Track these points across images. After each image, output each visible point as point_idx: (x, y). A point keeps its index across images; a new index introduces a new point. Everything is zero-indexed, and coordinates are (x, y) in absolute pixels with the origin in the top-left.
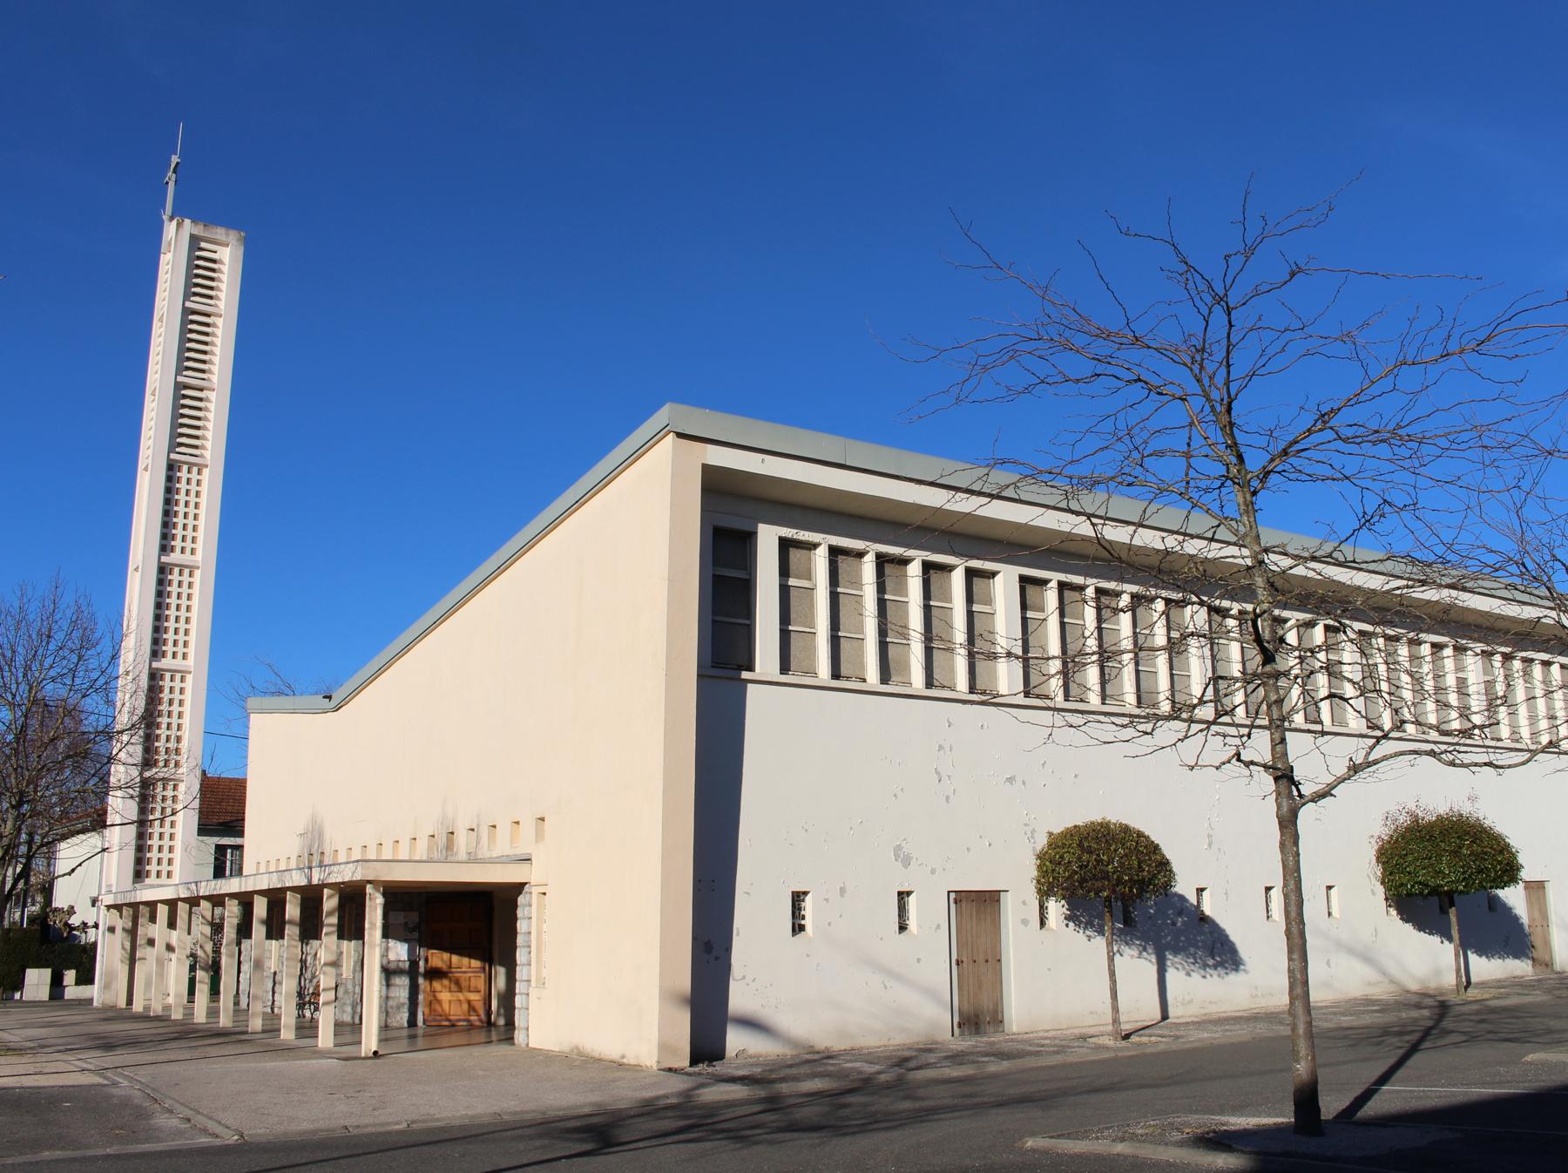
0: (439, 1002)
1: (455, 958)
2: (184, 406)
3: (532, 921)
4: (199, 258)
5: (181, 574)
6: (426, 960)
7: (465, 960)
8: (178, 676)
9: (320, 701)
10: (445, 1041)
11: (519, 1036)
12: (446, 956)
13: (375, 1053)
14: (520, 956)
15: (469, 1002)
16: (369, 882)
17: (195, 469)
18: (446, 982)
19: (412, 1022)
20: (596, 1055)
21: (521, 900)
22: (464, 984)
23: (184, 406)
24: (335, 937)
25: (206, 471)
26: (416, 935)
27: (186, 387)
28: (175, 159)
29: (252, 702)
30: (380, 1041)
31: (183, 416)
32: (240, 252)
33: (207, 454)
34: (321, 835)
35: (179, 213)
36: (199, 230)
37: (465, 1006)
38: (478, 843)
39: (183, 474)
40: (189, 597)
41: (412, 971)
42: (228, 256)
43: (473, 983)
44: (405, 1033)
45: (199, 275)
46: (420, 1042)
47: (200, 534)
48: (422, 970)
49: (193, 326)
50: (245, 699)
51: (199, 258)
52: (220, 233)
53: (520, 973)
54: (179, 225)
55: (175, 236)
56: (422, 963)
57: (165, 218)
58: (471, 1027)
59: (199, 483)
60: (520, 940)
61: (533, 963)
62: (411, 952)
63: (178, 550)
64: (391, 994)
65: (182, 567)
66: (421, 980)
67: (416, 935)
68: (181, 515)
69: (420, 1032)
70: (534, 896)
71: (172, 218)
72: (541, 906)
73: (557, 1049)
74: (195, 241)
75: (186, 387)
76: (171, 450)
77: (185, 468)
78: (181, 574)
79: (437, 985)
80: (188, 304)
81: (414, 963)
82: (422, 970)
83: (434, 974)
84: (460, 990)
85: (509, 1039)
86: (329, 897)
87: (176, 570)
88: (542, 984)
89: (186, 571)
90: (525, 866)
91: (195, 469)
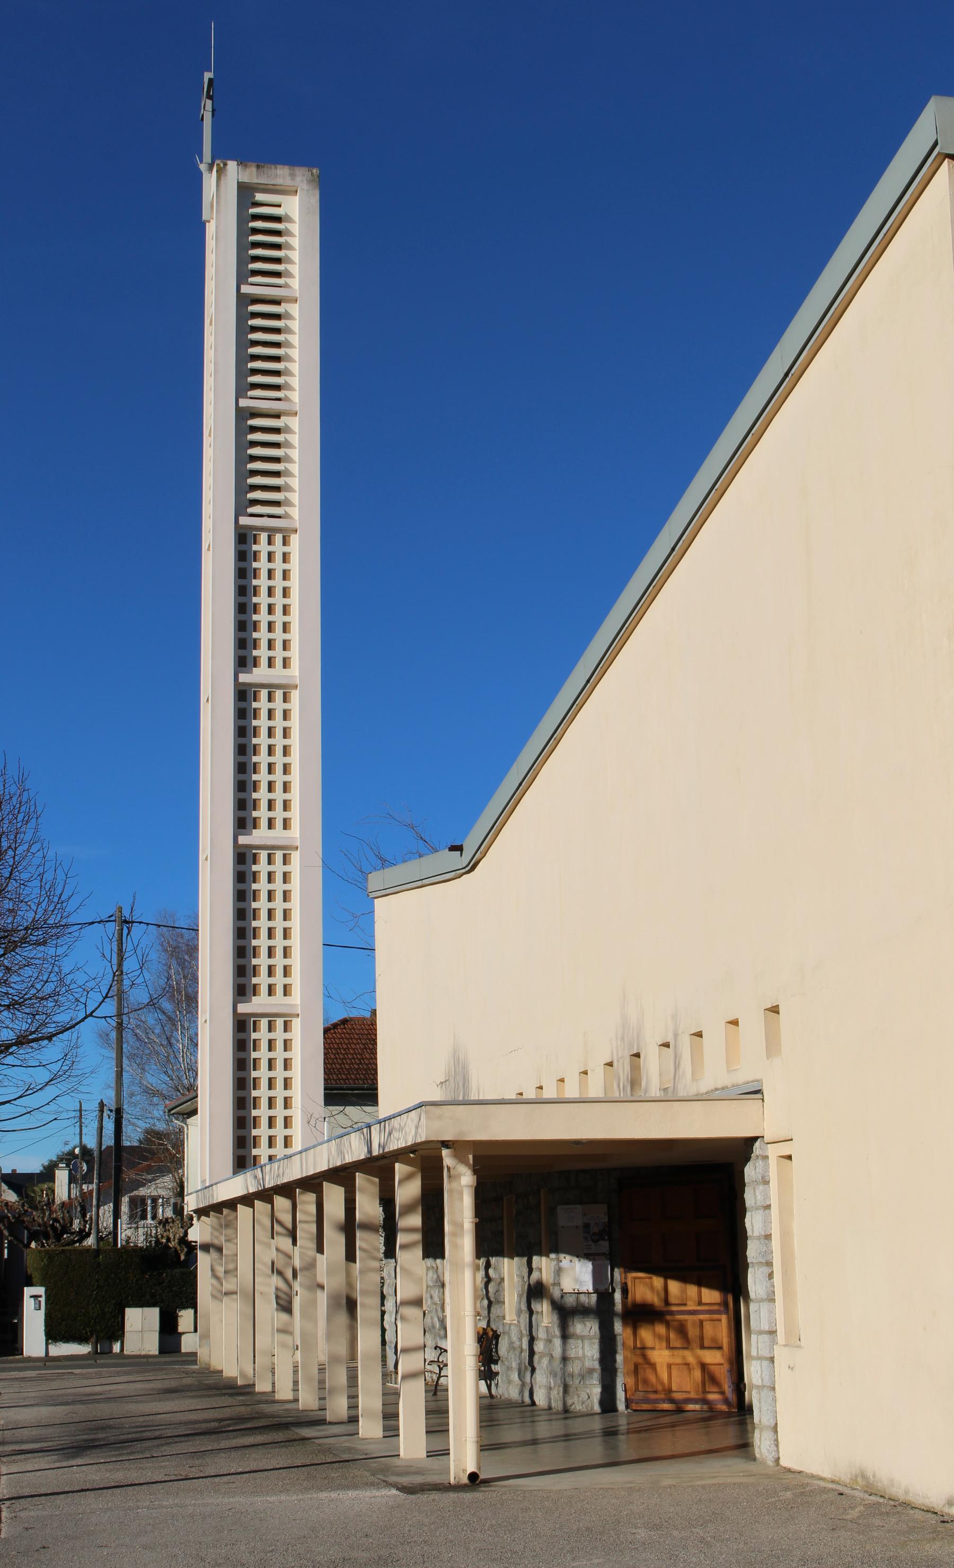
0: (653, 1366)
1: (674, 1287)
2: (254, 444)
3: (775, 1212)
4: (256, 217)
5: (270, 699)
6: (625, 1291)
7: (692, 1290)
8: (279, 855)
9: (457, 860)
10: (666, 1442)
11: (762, 1443)
12: (658, 1282)
13: (473, 1477)
14: (755, 1282)
15: (703, 1366)
16: (445, 1144)
17: (278, 538)
18: (661, 1329)
19: (608, 1404)
20: (898, 1492)
21: (750, 1172)
22: (693, 1332)
23: (254, 444)
24: (419, 1252)
25: (294, 539)
26: (604, 1246)
27: (255, 414)
28: (208, 76)
29: (375, 880)
30: (485, 1447)
31: (254, 458)
32: (314, 200)
33: (295, 512)
34: (466, 1080)
35: (222, 153)
36: (250, 175)
37: (697, 1374)
38: (677, 1066)
39: (262, 547)
40: (286, 733)
41: (602, 1310)
42: (297, 208)
43: (708, 1329)
44: (597, 1425)
45: (259, 243)
46: (626, 1446)
47: (294, 636)
48: (618, 1307)
49: (257, 322)
50: (365, 875)
51: (256, 217)
52: (281, 175)
53: (757, 1315)
54: (220, 172)
55: (219, 193)
56: (618, 1296)
57: (203, 167)
58: (711, 1415)
59: (286, 558)
60: (753, 1251)
61: (779, 1296)
62: (598, 1276)
63: (264, 662)
64: (572, 1353)
65: (271, 688)
66: (618, 1327)
67: (604, 1246)
68: (264, 609)
69: (623, 1423)
70: (773, 1162)
71: (211, 167)
72: (786, 1185)
73: (827, 1474)
74: (246, 192)
75: (255, 414)
76: (240, 511)
77: (264, 537)
78: (270, 699)
79: (646, 1335)
80: (245, 289)
81: (604, 1296)
82: (618, 1307)
83: (640, 1315)
84: (687, 1343)
85: (744, 1447)
86: (408, 1178)
87: (264, 694)
88: (794, 1342)
89: (279, 694)
90: (751, 1105)
91: (278, 538)
